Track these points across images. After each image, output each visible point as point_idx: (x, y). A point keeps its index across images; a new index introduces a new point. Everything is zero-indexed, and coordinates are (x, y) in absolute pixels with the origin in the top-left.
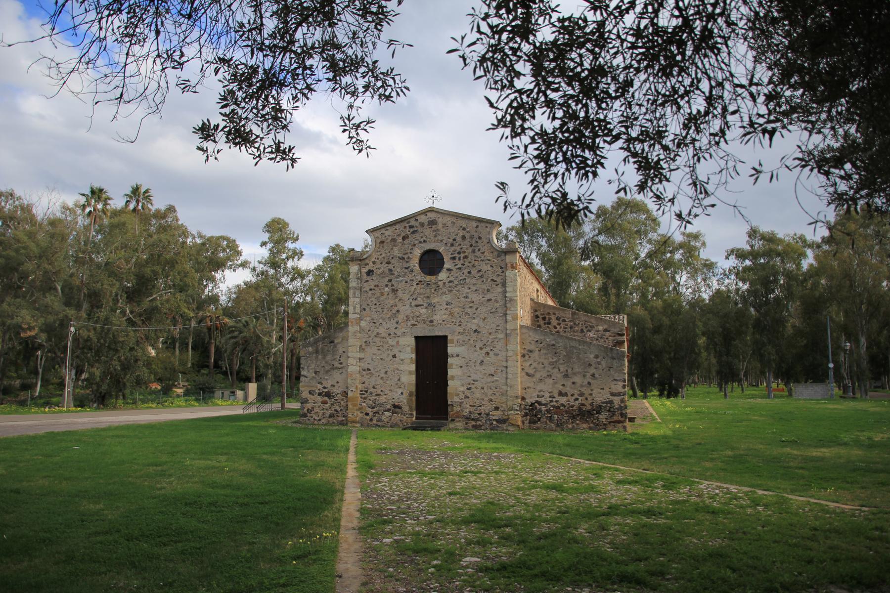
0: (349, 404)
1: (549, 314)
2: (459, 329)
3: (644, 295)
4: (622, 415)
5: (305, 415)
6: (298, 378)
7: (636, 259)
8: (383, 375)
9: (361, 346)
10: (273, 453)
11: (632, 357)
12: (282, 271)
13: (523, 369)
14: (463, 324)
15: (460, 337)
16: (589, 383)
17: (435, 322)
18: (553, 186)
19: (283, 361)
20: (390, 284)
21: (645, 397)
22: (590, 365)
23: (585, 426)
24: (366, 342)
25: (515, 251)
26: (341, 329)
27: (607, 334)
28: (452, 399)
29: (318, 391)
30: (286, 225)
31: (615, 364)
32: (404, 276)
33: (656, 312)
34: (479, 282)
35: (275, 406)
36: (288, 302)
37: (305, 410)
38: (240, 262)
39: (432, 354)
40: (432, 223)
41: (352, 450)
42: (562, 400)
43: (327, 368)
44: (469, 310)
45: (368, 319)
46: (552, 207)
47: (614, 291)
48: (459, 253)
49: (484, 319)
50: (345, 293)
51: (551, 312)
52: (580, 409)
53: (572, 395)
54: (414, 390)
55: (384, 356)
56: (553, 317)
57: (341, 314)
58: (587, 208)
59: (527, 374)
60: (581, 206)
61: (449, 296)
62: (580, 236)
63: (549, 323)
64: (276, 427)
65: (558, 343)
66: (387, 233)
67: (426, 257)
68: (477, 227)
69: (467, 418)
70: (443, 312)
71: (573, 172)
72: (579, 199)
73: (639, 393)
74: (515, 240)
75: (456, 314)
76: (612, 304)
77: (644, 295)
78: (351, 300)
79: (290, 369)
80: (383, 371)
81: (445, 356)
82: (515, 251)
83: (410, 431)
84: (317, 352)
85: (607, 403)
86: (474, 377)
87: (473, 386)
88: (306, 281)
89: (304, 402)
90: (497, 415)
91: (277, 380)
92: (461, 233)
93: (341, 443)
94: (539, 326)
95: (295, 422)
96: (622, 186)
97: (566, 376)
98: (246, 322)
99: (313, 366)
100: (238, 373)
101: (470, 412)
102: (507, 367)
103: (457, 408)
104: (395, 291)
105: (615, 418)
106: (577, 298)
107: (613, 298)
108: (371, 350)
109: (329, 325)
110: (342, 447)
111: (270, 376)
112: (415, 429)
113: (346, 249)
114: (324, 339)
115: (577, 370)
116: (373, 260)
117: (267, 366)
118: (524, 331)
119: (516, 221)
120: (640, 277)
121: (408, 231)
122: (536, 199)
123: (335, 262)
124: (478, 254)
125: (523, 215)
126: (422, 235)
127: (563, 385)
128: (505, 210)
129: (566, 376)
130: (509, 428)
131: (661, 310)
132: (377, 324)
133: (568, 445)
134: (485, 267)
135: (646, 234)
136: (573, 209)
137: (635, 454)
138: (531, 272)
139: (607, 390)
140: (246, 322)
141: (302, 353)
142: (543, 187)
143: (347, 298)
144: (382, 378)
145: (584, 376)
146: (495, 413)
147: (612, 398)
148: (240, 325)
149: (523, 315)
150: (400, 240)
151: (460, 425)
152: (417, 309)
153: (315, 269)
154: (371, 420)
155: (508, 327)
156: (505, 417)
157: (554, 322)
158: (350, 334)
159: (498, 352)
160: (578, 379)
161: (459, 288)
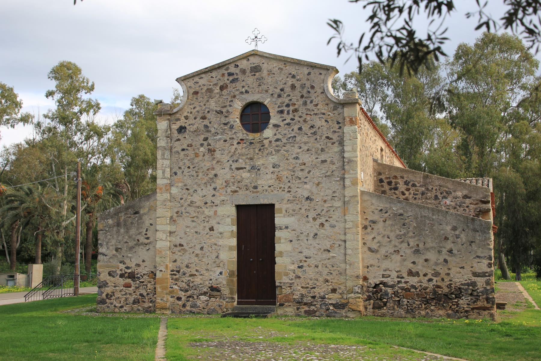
0: (158, 286)
1: (396, 177)
2: (287, 196)
3: (515, 154)
4: (488, 300)
5: (103, 302)
6: (95, 257)
7: (505, 109)
8: (198, 251)
9: (171, 217)
10: (62, 351)
11: (500, 230)
12: (74, 127)
13: (364, 244)
14: (293, 190)
15: (289, 205)
16: (446, 261)
17: (260, 189)
18: (397, 22)
19: (76, 237)
20: (205, 143)
21: (518, 279)
22: (446, 239)
23: (441, 312)
24: (177, 213)
25: (355, 103)
26: (148, 197)
27: (468, 201)
28: (281, 278)
29: (119, 272)
30: (77, 70)
31: (478, 237)
32: (222, 134)
33: (530, 174)
34: (312, 139)
35: (66, 291)
36: (82, 165)
37: (104, 295)
38: (19, 116)
39: (256, 226)
40: (256, 69)
41: (160, 343)
42: (413, 281)
43: (131, 244)
44: (300, 174)
45: (180, 185)
46: (395, 48)
47: (476, 149)
48: (288, 106)
49: (318, 184)
50: (153, 154)
51: (398, 175)
52: (435, 292)
53: (425, 275)
54: (235, 268)
55: (200, 229)
56: (400, 181)
57: (147, 179)
58: (438, 49)
59: (370, 249)
60: (432, 47)
61: (275, 157)
62: (435, 82)
63: (396, 189)
64: (67, 318)
65: (407, 212)
66: (201, 82)
67: (248, 111)
68: (309, 74)
69: (298, 302)
70: (269, 176)
71: (423, 5)
72: (429, 38)
73: (510, 274)
74: (355, 90)
75: (284, 178)
76: (474, 165)
77: (515, 154)
78: (160, 163)
79: (85, 246)
80: (198, 247)
81: (273, 228)
82: (355, 103)
83: (231, 319)
84: (118, 225)
85: (468, 284)
86: (306, 253)
87: (305, 264)
88: (104, 140)
89: (102, 285)
90: (334, 298)
91: (69, 259)
92: (290, 81)
93: (146, 334)
94: (384, 192)
95: (91, 311)
96: (484, 19)
97: (417, 252)
98: (29, 189)
99: (113, 242)
100: (19, 252)
101: (302, 296)
102: (345, 241)
103: (286, 291)
104: (211, 151)
105: (479, 304)
106: (430, 158)
107: (475, 157)
108: (184, 222)
109: (133, 193)
110: (148, 339)
111: (60, 255)
112: (236, 316)
113: (152, 101)
114: (127, 209)
115: (430, 244)
116: (185, 114)
117: (56, 243)
118: (366, 198)
119: (354, 67)
120: (510, 132)
121: (226, 80)
122: (376, 40)
123: (140, 117)
124: (310, 106)
125: (360, 59)
126: (244, 84)
127: (414, 263)
128: (339, 53)
129: (417, 252)
130: (349, 314)
131: (537, 171)
132: (191, 191)
133: (421, 336)
134: (319, 122)
135: (519, 77)
136: (421, 51)
137: (506, 350)
138: (374, 128)
139: (468, 269)
140: (29, 189)
141: (100, 227)
142: (385, 24)
143: (155, 160)
144: (197, 255)
145: (440, 252)
146: (331, 295)
147: (474, 279)
148: (21, 193)
149: (364, 178)
150: (217, 90)
151: (290, 310)
152: (238, 172)
153: (116, 126)
154: (184, 306)
155: (346, 194)
156: (344, 301)
157: (402, 187)
158: (158, 203)
159: (335, 223)
160: (432, 256)
161: (288, 147)
